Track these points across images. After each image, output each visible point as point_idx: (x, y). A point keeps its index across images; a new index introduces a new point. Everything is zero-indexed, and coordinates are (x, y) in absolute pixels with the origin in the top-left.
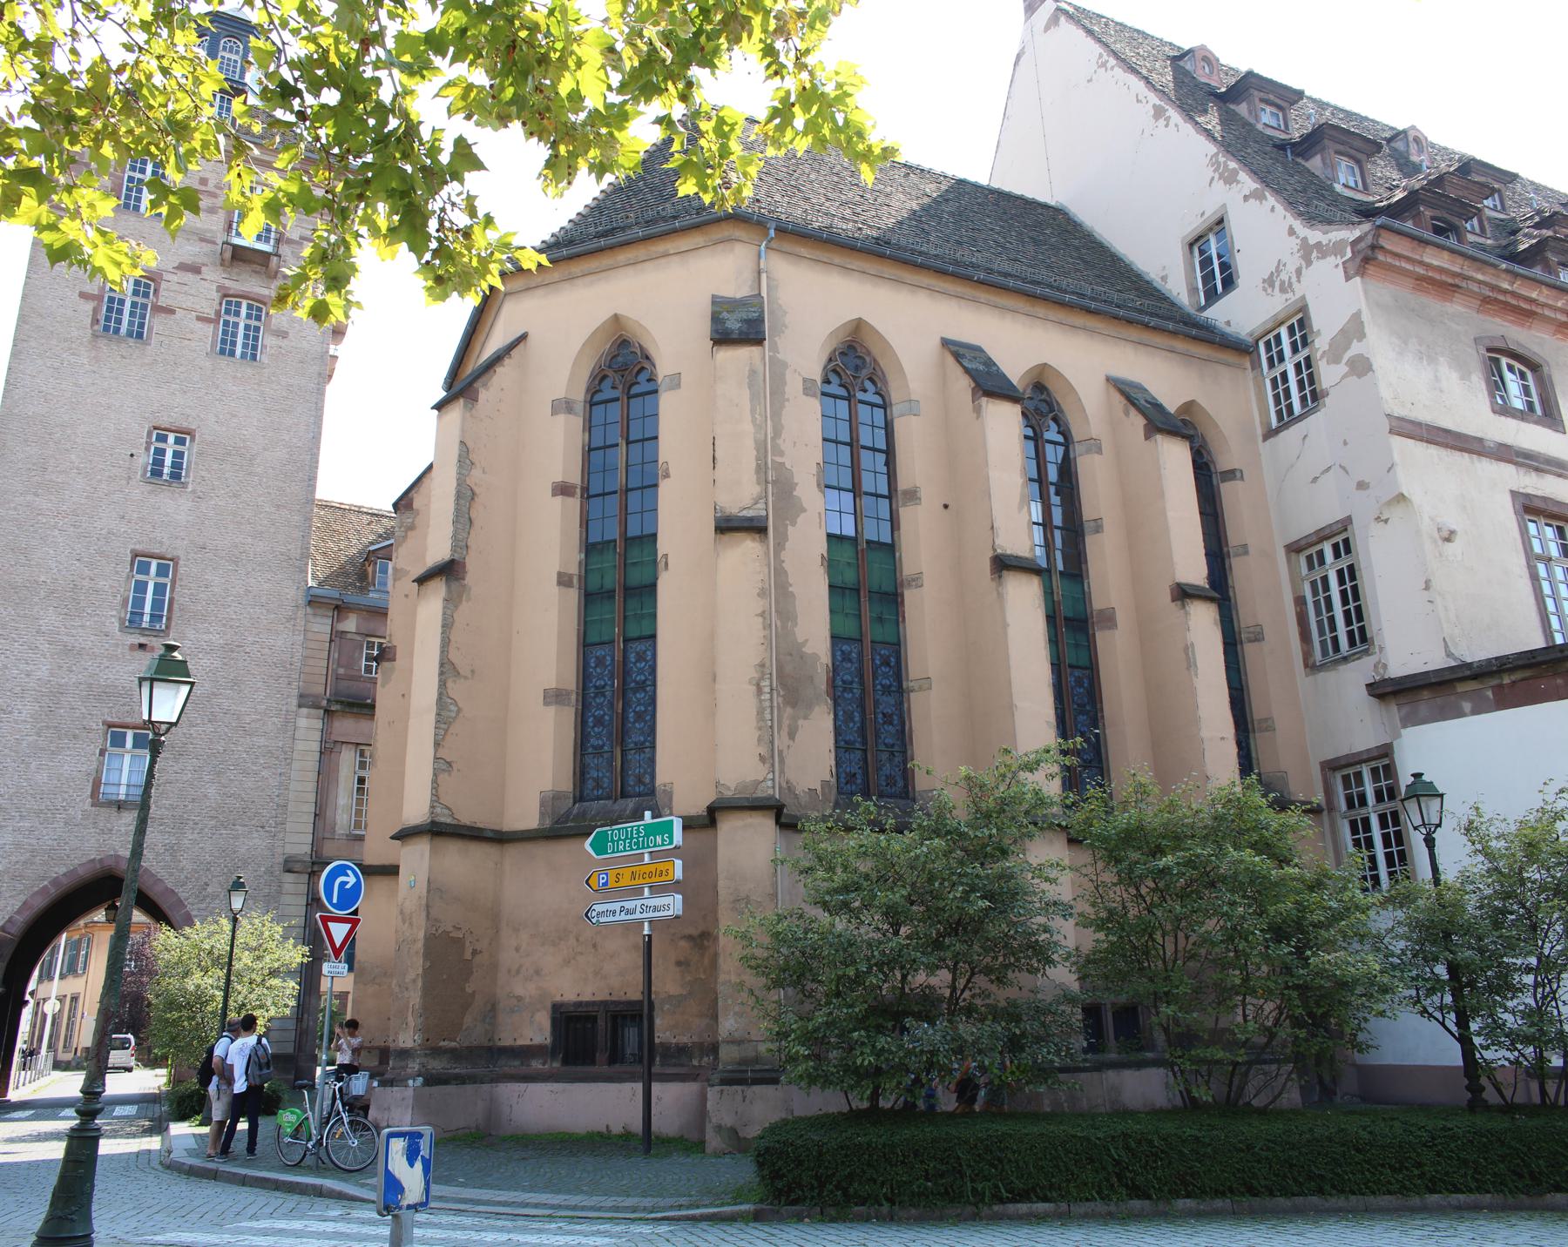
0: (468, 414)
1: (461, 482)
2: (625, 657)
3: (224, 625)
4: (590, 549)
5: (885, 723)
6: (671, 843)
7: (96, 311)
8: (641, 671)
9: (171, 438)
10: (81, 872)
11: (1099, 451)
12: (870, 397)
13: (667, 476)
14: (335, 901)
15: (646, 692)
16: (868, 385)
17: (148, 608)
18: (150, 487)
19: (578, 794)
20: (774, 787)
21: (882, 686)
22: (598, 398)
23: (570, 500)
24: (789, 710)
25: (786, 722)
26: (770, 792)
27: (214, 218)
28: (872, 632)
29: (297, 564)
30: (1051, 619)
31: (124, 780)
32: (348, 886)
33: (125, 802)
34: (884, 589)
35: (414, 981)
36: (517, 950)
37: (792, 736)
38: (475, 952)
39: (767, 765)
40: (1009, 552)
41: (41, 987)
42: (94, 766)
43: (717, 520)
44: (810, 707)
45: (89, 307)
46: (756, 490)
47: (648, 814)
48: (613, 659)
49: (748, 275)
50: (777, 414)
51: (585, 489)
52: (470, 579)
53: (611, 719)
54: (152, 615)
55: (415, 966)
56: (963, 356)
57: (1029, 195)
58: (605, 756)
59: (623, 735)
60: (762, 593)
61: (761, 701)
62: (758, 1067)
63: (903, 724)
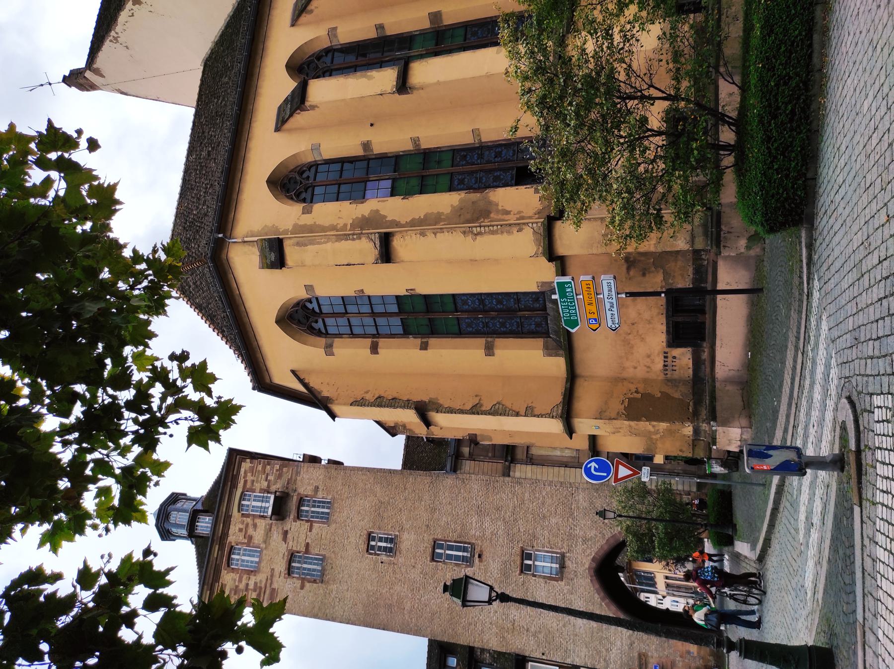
0: (336, 402)
1: (372, 405)
2: (466, 311)
3: (468, 515)
4: (407, 332)
5: (500, 157)
6: (570, 283)
7: (309, 582)
8: (473, 302)
9: (373, 543)
10: (597, 586)
11: (335, 29)
12: (311, 174)
13: (362, 291)
14: (605, 474)
15: (485, 299)
16: (305, 175)
17: (460, 554)
18: (398, 553)
19: (545, 336)
20: (537, 223)
21: (478, 159)
22: (324, 331)
23: (380, 344)
24: (492, 215)
25: (500, 217)
26: (539, 224)
27: (258, 524)
28: (446, 167)
29: (434, 478)
30: (436, 54)
31: (549, 565)
32: (597, 467)
33: (560, 564)
34: (421, 161)
35: (654, 426)
36: (635, 368)
37: (508, 213)
38: (637, 392)
39: (524, 227)
40: (395, 83)
41: (660, 593)
42: (541, 580)
43: (383, 262)
44: (490, 203)
45: (307, 585)
46: (364, 240)
47: (554, 297)
48: (467, 318)
49: (246, 248)
50: (323, 229)
51: (374, 336)
52: (426, 399)
53: (501, 318)
54: (464, 551)
55: (645, 425)
56: (283, 118)
57: (198, 83)
58: (523, 320)
59: (509, 310)
60: (423, 234)
61: (485, 232)
62: (710, 225)
63: (501, 145)
